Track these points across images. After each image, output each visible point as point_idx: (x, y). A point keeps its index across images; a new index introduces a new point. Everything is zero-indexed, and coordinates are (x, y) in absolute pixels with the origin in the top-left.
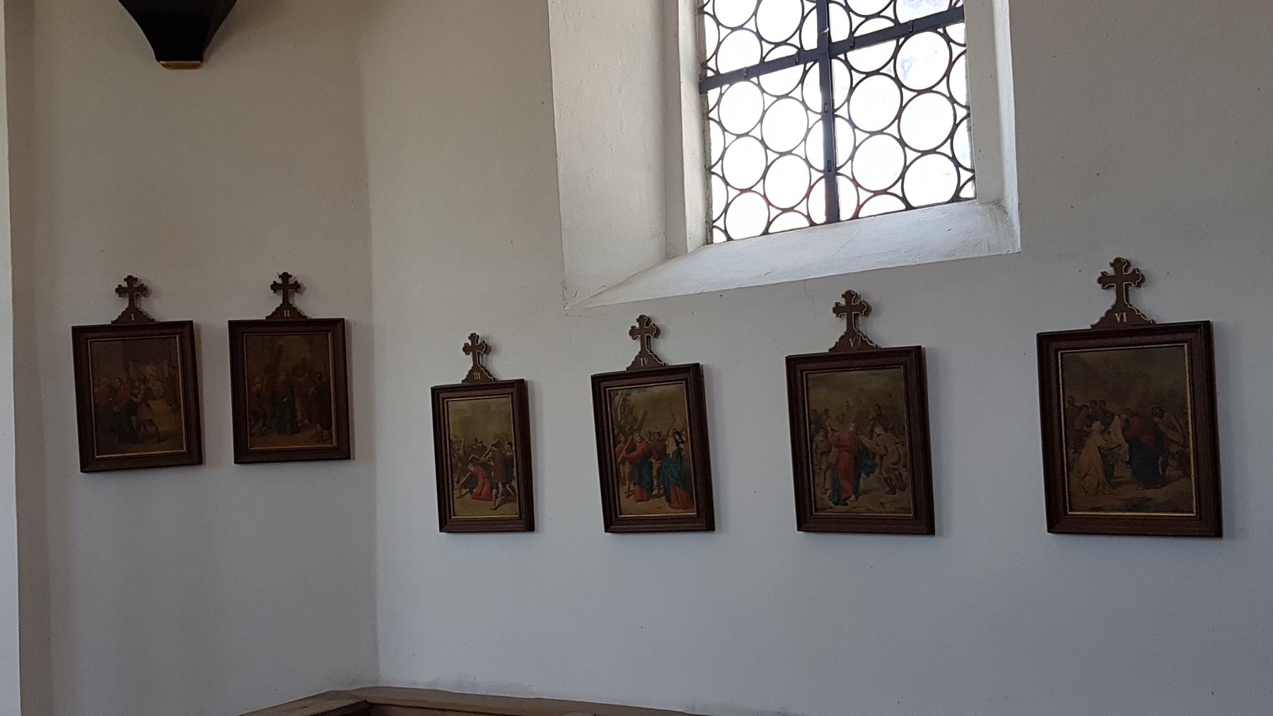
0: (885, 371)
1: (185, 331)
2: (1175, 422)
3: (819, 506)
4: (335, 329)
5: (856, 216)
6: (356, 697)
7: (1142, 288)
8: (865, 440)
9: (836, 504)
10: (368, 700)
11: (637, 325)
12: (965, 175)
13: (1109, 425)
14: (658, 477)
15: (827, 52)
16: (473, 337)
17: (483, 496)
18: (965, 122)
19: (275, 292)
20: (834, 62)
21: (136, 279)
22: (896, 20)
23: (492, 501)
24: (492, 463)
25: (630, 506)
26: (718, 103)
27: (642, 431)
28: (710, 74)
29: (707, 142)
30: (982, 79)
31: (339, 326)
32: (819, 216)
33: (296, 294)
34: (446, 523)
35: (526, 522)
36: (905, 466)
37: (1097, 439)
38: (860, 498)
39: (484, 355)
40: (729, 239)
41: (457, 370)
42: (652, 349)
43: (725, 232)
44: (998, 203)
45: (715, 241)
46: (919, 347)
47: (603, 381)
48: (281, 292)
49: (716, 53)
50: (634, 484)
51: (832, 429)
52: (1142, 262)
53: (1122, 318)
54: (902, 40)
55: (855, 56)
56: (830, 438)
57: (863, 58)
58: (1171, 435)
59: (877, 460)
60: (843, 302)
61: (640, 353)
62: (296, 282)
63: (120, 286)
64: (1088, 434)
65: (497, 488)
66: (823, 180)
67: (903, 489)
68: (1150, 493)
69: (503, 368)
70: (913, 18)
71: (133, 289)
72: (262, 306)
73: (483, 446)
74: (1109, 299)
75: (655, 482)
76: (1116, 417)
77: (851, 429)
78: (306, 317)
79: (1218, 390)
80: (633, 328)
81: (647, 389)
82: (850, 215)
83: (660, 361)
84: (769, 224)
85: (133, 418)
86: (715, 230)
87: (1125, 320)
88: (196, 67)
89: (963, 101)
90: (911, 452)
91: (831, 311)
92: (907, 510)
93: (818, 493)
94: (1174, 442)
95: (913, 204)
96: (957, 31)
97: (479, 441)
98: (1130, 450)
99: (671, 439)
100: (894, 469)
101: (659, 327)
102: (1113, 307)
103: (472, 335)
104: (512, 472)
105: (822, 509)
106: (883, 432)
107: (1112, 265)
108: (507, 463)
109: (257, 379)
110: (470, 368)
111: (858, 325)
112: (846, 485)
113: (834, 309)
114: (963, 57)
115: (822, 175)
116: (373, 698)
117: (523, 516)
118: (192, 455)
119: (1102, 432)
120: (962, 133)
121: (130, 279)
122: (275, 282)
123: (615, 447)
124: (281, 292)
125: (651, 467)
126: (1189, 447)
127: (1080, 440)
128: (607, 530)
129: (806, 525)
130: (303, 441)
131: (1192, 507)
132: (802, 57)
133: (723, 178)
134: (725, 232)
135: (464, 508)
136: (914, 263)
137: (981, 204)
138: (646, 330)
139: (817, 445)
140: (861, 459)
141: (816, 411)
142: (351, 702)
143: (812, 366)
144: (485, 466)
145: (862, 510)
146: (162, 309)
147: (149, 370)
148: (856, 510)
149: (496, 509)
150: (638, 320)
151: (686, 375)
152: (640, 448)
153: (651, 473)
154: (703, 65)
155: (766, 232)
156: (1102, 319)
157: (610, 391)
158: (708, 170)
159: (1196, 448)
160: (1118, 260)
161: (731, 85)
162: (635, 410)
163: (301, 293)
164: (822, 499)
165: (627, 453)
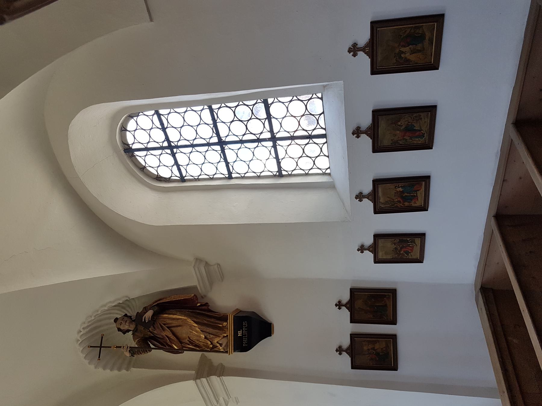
0: (379, 122)
1: (353, 336)
2: (404, 31)
3: (424, 142)
4: (353, 291)
5: (325, 129)
6: (478, 292)
7: (358, 43)
8: (403, 127)
9: (424, 137)
10: (479, 288)
11: (358, 199)
12: (314, 96)
13: (403, 52)
14: (410, 194)
15: (274, 139)
16: (358, 250)
17: (412, 249)
18: (298, 97)
19: (341, 309)
20: (276, 137)
21: (337, 349)
22: (266, 119)
23: (413, 246)
24: (401, 246)
25: (420, 202)
26: (287, 171)
27: (394, 198)
28: (278, 174)
29: (299, 175)
30: (284, 94)
31: (352, 290)
32: (324, 140)
33: (342, 302)
34: (421, 261)
35: (422, 236)
36: (412, 115)
37: (408, 56)
38: (422, 129)
39: (364, 247)
40: (329, 168)
41: (369, 256)
42: (366, 195)
43: (327, 169)
44: (324, 86)
45: (329, 172)
46: (372, 111)
47: (376, 210)
48: (341, 307)
49: (272, 172)
50: (412, 201)
51: (398, 138)
52: (349, 44)
53: (367, 49)
54: (272, 117)
55: (275, 131)
56: (401, 139)
57: (276, 127)
58: (408, 32)
59: (410, 124)
60: (355, 135)
61: (367, 199)
62: (338, 302)
63: (339, 354)
64: (406, 58)
65: (410, 244)
66: (312, 139)
67: (420, 116)
68: (427, 38)
69: (369, 241)
70: (265, 114)
71: (340, 350)
72: (346, 313)
73: (395, 248)
74: (361, 54)
75: (412, 194)
76: (400, 50)
77: (399, 132)
78: (349, 300)
79: (393, 18)
80: (359, 201)
81: (380, 196)
82: (324, 131)
83: (370, 192)
84: (325, 156)
85: (381, 354)
86: (326, 172)
87: (368, 48)
88: (273, 325)
89: (291, 98)
90: (408, 113)
91: (358, 139)
92: (427, 116)
93: (420, 142)
94: (410, 31)
95: (322, 111)
96: (270, 101)
97: (393, 249)
98: (412, 45)
99: (397, 189)
100: (413, 118)
101: (359, 192)
102: (363, 52)
103: (357, 250)
104: (404, 240)
105: (426, 141)
106: (400, 122)
107: (350, 53)
108: (401, 241)
109: (369, 316)
110: (368, 251)
111: (363, 130)
112: (417, 133)
113: (357, 138)
114: (278, 98)
115: (311, 140)
116: (479, 287)
117: (420, 237)
118: (394, 337)
119: (405, 54)
120: (301, 98)
121: (337, 351)
122: (338, 308)
123: (398, 207)
124: (341, 307)
125: (407, 196)
126: (412, 26)
127: (407, 61)
128: (427, 210)
129: (431, 146)
130: (390, 304)
131: (433, 24)
132: (275, 146)
133: (310, 170)
134: (327, 169)
135: (416, 254)
136: (344, 114)
137: (324, 91)
138: (360, 197)
139: (403, 143)
140: (409, 129)
141: (391, 143)
142: (480, 294)
143: (376, 145)
144: (401, 248)
145: (426, 128)
146: (346, 342)
147: (365, 348)
148: (426, 130)
149: (417, 245)
150: (357, 199)
151: (376, 184)
152: (399, 199)
153: (408, 196)
154: (275, 176)
155: (328, 157)
156: (367, 55)
157: (379, 208)
158: (307, 174)
159: (412, 24)
160: (348, 51)
161: (281, 167)
162: (386, 201)
163: (341, 301)
164: (422, 141)
165: (401, 203)
